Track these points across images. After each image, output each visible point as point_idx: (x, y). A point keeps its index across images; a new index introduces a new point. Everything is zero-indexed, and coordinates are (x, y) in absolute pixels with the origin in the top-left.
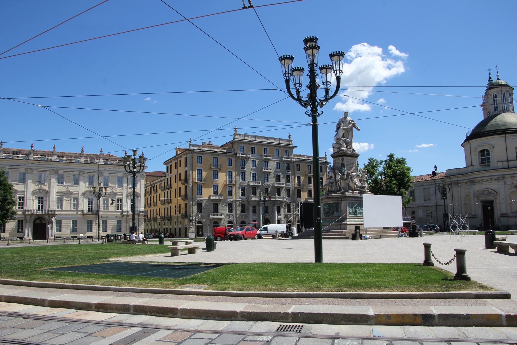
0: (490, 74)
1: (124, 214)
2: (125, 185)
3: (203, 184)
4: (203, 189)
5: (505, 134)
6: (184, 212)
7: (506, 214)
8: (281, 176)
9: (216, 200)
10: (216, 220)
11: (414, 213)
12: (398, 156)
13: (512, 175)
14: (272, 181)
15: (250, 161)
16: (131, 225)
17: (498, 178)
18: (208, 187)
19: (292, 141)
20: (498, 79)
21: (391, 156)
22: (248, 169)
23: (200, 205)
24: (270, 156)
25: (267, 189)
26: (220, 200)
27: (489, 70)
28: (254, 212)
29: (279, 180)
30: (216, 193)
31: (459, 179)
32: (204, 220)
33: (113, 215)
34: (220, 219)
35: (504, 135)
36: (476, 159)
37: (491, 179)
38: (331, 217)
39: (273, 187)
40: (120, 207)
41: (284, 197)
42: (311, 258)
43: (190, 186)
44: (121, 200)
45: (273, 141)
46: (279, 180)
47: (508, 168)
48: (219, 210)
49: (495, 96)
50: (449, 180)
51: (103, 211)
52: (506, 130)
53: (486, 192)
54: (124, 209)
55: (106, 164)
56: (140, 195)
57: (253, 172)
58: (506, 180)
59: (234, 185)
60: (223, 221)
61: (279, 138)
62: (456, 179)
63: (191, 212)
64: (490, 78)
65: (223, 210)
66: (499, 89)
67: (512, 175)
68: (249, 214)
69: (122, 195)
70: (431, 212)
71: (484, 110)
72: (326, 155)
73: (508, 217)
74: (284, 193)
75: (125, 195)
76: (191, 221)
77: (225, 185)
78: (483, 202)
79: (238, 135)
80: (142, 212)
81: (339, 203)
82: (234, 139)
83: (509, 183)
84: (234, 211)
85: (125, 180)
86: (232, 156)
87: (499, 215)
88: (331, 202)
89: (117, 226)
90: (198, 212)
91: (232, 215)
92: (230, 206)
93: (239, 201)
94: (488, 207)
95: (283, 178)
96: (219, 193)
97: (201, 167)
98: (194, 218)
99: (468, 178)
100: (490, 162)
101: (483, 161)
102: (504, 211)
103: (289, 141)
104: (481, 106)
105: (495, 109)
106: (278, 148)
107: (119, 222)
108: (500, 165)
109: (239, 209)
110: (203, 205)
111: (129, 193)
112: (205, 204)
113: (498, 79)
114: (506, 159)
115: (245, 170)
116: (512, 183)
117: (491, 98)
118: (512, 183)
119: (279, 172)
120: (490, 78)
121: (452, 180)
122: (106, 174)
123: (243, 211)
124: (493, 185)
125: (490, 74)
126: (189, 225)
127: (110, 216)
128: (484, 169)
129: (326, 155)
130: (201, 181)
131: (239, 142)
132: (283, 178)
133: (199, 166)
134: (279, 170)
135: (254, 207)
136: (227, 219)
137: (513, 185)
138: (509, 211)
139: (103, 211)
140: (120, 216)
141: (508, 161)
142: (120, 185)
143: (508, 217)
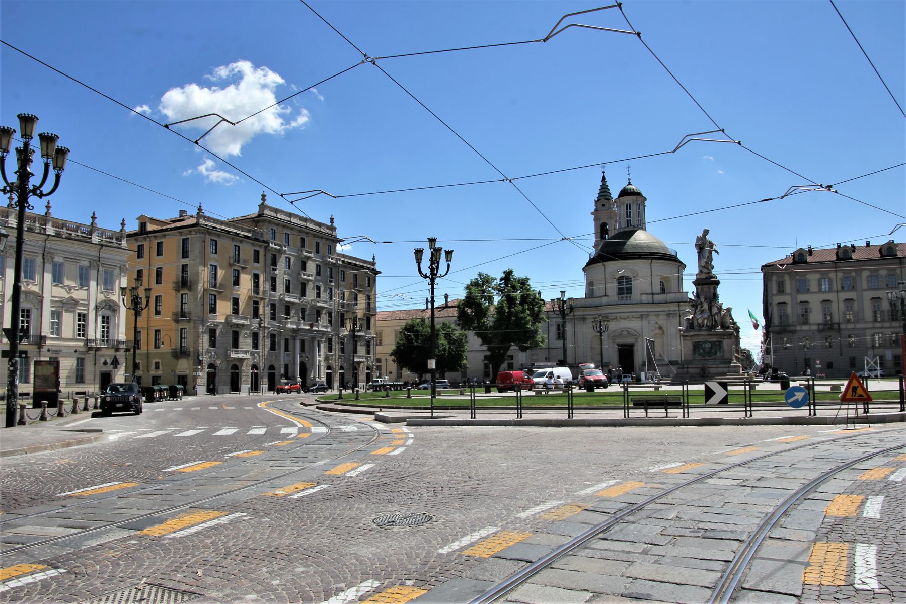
1: (90, 345)
2: (93, 284)
3: (219, 293)
4: (218, 302)
8: (322, 289)
9: (237, 325)
10: (235, 363)
12: (518, 274)
14: (310, 295)
15: (284, 256)
18: (225, 299)
19: (335, 228)
20: (629, 184)
21: (508, 274)
22: (281, 273)
23: (212, 332)
24: (310, 253)
25: (303, 311)
26: (243, 325)
28: (287, 349)
29: (318, 295)
30: (236, 311)
31: (586, 313)
32: (218, 362)
33: (70, 347)
34: (241, 360)
39: (313, 307)
40: (82, 330)
41: (323, 326)
42: (644, 415)
43: (200, 296)
44: (84, 315)
45: (313, 226)
46: (318, 295)
48: (240, 344)
49: (628, 207)
51: (52, 339)
52: (651, 253)
53: (625, 333)
54: (91, 334)
55: (58, 235)
56: (118, 306)
57: (286, 277)
58: (650, 318)
59: (262, 299)
60: (244, 364)
61: (320, 221)
63: (201, 345)
64: (604, 178)
65: (246, 342)
66: (634, 197)
68: (280, 353)
69: (88, 305)
70: (379, 361)
71: (596, 220)
72: (374, 259)
74: (324, 318)
75: (92, 305)
76: (200, 363)
77: (250, 298)
78: (618, 345)
79: (268, 207)
80: (123, 342)
82: (260, 215)
84: (260, 347)
85: (93, 273)
86: (260, 246)
89: (77, 370)
90: (210, 345)
91: (258, 353)
92: (255, 336)
93: (268, 328)
95: (325, 291)
96: (240, 312)
97: (216, 260)
98: (205, 359)
99: (598, 312)
100: (631, 293)
101: (620, 291)
103: (333, 228)
104: (592, 214)
105: (629, 223)
106: (319, 240)
107: (81, 362)
108: (644, 298)
109: (268, 343)
110: (218, 333)
111: (101, 303)
112: (221, 332)
113: (629, 184)
114: (650, 292)
115: (277, 272)
117: (623, 208)
119: (318, 281)
120: (604, 178)
122: (58, 259)
123: (273, 348)
124: (635, 325)
126: (196, 370)
127: (64, 350)
128: (622, 302)
129: (374, 259)
130: (215, 286)
131: (270, 222)
132: (325, 291)
133: (213, 259)
134: (318, 278)
135: (287, 341)
136: (250, 363)
138: (679, 360)
139: (52, 339)
140: (84, 350)
141: (653, 294)
142: (84, 282)
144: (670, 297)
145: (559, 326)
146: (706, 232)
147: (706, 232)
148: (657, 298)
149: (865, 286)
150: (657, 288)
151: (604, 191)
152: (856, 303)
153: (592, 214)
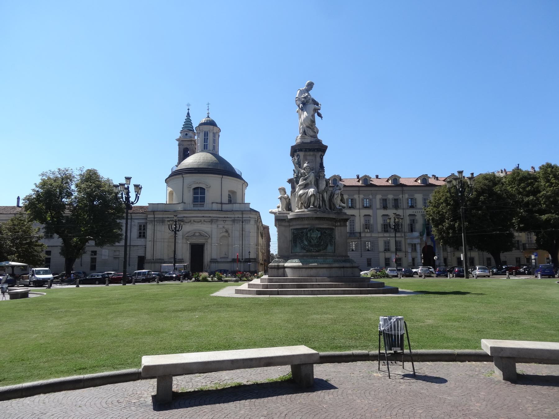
0: (188, 109)
5: (223, 175)
6: (320, 182)
7: (216, 259)
11: (95, 254)
13: (225, 219)
16: (400, 290)
17: (211, 221)
27: (188, 105)
31: (164, 216)
35: (221, 176)
36: (189, 196)
37: (204, 221)
38: (322, 253)
47: (222, 211)
50: (152, 216)
62: (161, 216)
64: (188, 114)
67: (225, 219)
71: (179, 145)
73: (218, 262)
81: (333, 229)
83: (221, 226)
87: (209, 260)
88: (325, 226)
94: (197, 251)
101: (195, 200)
102: (214, 256)
108: (215, 207)
114: (220, 201)
116: (224, 227)
118: (224, 227)
120: (188, 114)
121: (156, 216)
124: (206, 228)
125: (188, 109)
137: (224, 230)
138: (240, 257)
141: (222, 203)
143: (218, 262)
144: (236, 207)
145: (140, 226)
146: (310, 86)
147: (310, 86)
148: (225, 207)
149: (378, 206)
150: (225, 199)
151: (188, 124)
152: (372, 218)
153: (177, 140)
